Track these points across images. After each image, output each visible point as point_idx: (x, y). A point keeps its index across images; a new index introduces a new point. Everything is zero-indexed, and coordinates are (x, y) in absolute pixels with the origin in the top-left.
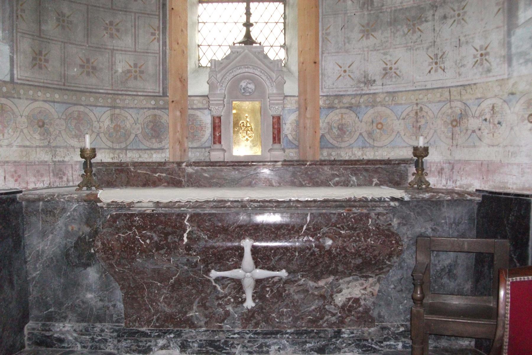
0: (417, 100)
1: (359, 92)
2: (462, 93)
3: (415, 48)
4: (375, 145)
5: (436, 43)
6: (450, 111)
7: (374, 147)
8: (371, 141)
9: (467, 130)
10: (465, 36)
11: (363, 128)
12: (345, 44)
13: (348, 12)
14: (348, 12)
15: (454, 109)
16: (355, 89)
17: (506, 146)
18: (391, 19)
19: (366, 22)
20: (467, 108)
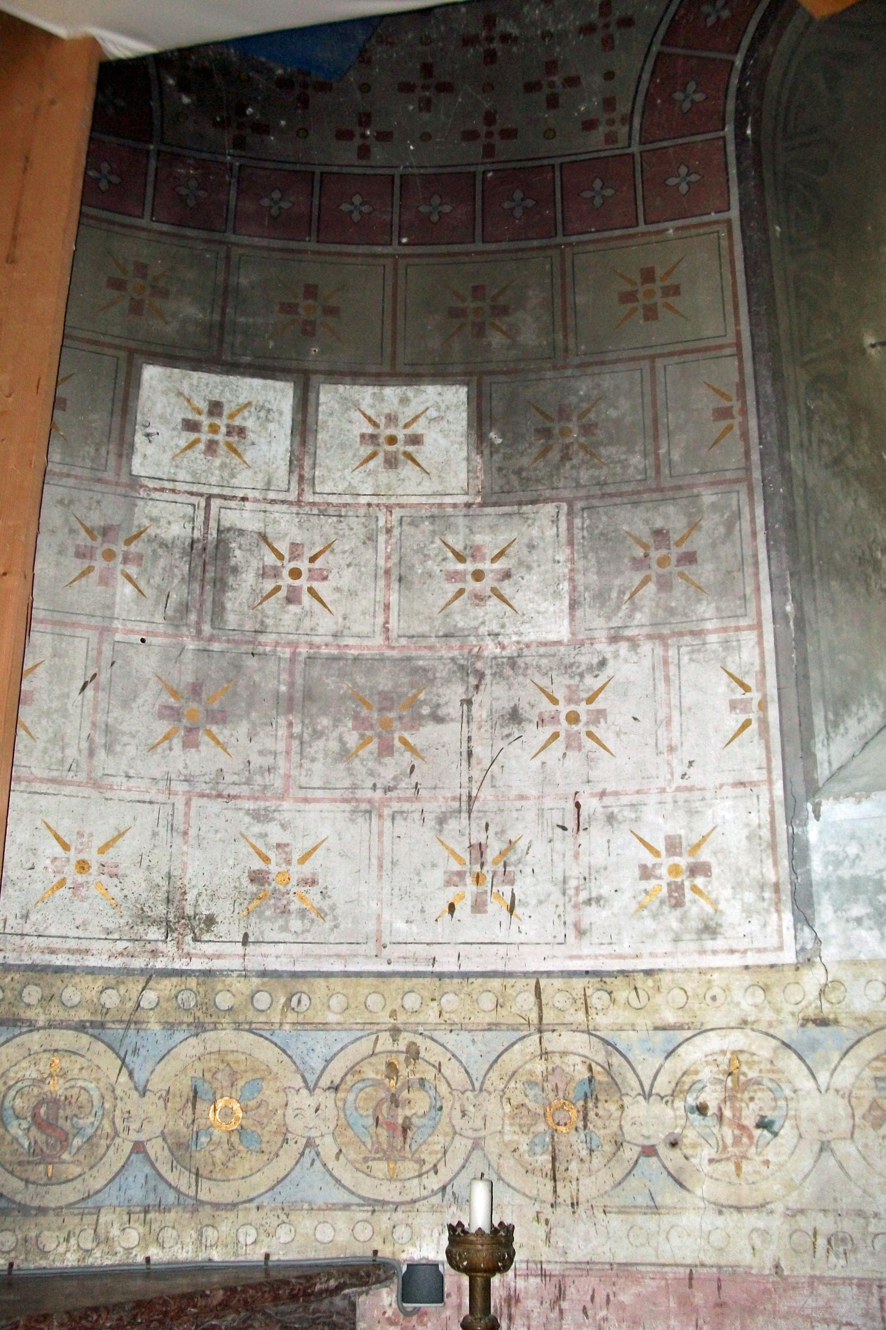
0: (393, 1014)
1: (138, 963)
2: (594, 1001)
3: (387, 812)
4: (203, 1196)
5: (476, 806)
6: (539, 1067)
7: (197, 1205)
8: (183, 1181)
9: (619, 1145)
10: (603, 794)
11: (152, 1120)
12: (91, 753)
13: (117, 624)
14: (117, 624)
15: (557, 1060)
16: (121, 946)
17: (802, 1211)
18: (291, 685)
19: (189, 678)
20: (616, 1060)
